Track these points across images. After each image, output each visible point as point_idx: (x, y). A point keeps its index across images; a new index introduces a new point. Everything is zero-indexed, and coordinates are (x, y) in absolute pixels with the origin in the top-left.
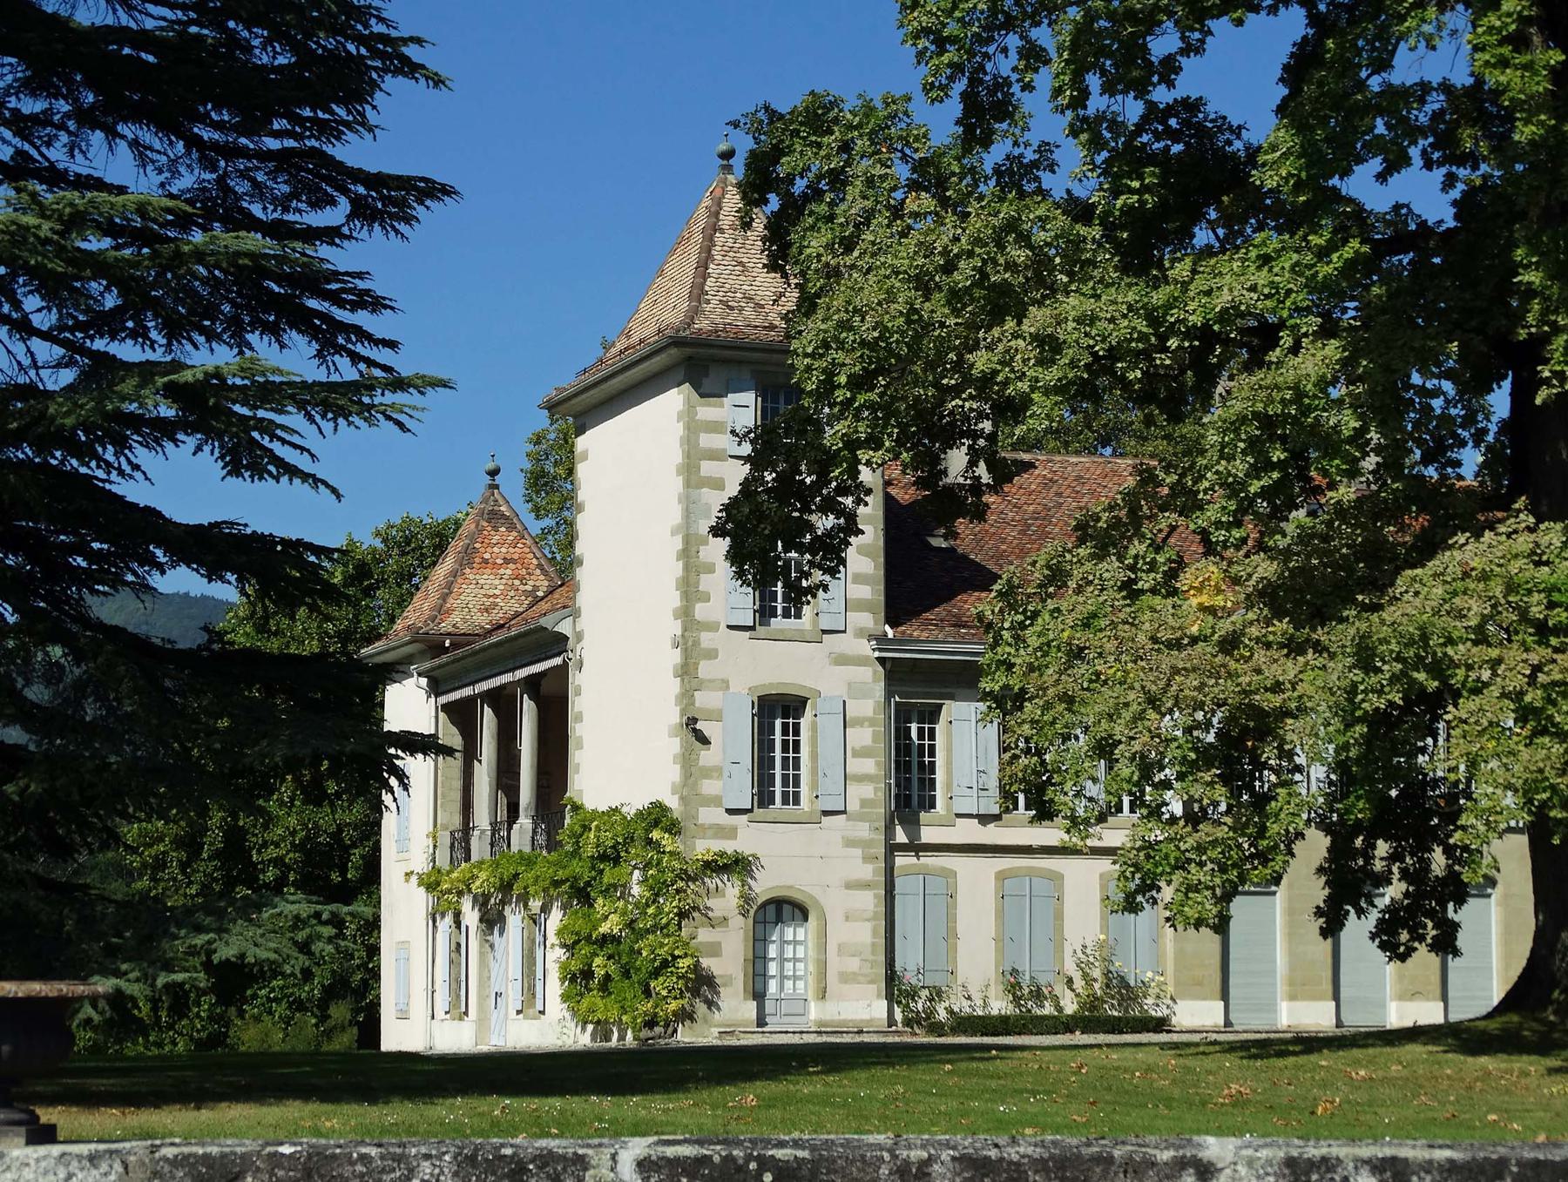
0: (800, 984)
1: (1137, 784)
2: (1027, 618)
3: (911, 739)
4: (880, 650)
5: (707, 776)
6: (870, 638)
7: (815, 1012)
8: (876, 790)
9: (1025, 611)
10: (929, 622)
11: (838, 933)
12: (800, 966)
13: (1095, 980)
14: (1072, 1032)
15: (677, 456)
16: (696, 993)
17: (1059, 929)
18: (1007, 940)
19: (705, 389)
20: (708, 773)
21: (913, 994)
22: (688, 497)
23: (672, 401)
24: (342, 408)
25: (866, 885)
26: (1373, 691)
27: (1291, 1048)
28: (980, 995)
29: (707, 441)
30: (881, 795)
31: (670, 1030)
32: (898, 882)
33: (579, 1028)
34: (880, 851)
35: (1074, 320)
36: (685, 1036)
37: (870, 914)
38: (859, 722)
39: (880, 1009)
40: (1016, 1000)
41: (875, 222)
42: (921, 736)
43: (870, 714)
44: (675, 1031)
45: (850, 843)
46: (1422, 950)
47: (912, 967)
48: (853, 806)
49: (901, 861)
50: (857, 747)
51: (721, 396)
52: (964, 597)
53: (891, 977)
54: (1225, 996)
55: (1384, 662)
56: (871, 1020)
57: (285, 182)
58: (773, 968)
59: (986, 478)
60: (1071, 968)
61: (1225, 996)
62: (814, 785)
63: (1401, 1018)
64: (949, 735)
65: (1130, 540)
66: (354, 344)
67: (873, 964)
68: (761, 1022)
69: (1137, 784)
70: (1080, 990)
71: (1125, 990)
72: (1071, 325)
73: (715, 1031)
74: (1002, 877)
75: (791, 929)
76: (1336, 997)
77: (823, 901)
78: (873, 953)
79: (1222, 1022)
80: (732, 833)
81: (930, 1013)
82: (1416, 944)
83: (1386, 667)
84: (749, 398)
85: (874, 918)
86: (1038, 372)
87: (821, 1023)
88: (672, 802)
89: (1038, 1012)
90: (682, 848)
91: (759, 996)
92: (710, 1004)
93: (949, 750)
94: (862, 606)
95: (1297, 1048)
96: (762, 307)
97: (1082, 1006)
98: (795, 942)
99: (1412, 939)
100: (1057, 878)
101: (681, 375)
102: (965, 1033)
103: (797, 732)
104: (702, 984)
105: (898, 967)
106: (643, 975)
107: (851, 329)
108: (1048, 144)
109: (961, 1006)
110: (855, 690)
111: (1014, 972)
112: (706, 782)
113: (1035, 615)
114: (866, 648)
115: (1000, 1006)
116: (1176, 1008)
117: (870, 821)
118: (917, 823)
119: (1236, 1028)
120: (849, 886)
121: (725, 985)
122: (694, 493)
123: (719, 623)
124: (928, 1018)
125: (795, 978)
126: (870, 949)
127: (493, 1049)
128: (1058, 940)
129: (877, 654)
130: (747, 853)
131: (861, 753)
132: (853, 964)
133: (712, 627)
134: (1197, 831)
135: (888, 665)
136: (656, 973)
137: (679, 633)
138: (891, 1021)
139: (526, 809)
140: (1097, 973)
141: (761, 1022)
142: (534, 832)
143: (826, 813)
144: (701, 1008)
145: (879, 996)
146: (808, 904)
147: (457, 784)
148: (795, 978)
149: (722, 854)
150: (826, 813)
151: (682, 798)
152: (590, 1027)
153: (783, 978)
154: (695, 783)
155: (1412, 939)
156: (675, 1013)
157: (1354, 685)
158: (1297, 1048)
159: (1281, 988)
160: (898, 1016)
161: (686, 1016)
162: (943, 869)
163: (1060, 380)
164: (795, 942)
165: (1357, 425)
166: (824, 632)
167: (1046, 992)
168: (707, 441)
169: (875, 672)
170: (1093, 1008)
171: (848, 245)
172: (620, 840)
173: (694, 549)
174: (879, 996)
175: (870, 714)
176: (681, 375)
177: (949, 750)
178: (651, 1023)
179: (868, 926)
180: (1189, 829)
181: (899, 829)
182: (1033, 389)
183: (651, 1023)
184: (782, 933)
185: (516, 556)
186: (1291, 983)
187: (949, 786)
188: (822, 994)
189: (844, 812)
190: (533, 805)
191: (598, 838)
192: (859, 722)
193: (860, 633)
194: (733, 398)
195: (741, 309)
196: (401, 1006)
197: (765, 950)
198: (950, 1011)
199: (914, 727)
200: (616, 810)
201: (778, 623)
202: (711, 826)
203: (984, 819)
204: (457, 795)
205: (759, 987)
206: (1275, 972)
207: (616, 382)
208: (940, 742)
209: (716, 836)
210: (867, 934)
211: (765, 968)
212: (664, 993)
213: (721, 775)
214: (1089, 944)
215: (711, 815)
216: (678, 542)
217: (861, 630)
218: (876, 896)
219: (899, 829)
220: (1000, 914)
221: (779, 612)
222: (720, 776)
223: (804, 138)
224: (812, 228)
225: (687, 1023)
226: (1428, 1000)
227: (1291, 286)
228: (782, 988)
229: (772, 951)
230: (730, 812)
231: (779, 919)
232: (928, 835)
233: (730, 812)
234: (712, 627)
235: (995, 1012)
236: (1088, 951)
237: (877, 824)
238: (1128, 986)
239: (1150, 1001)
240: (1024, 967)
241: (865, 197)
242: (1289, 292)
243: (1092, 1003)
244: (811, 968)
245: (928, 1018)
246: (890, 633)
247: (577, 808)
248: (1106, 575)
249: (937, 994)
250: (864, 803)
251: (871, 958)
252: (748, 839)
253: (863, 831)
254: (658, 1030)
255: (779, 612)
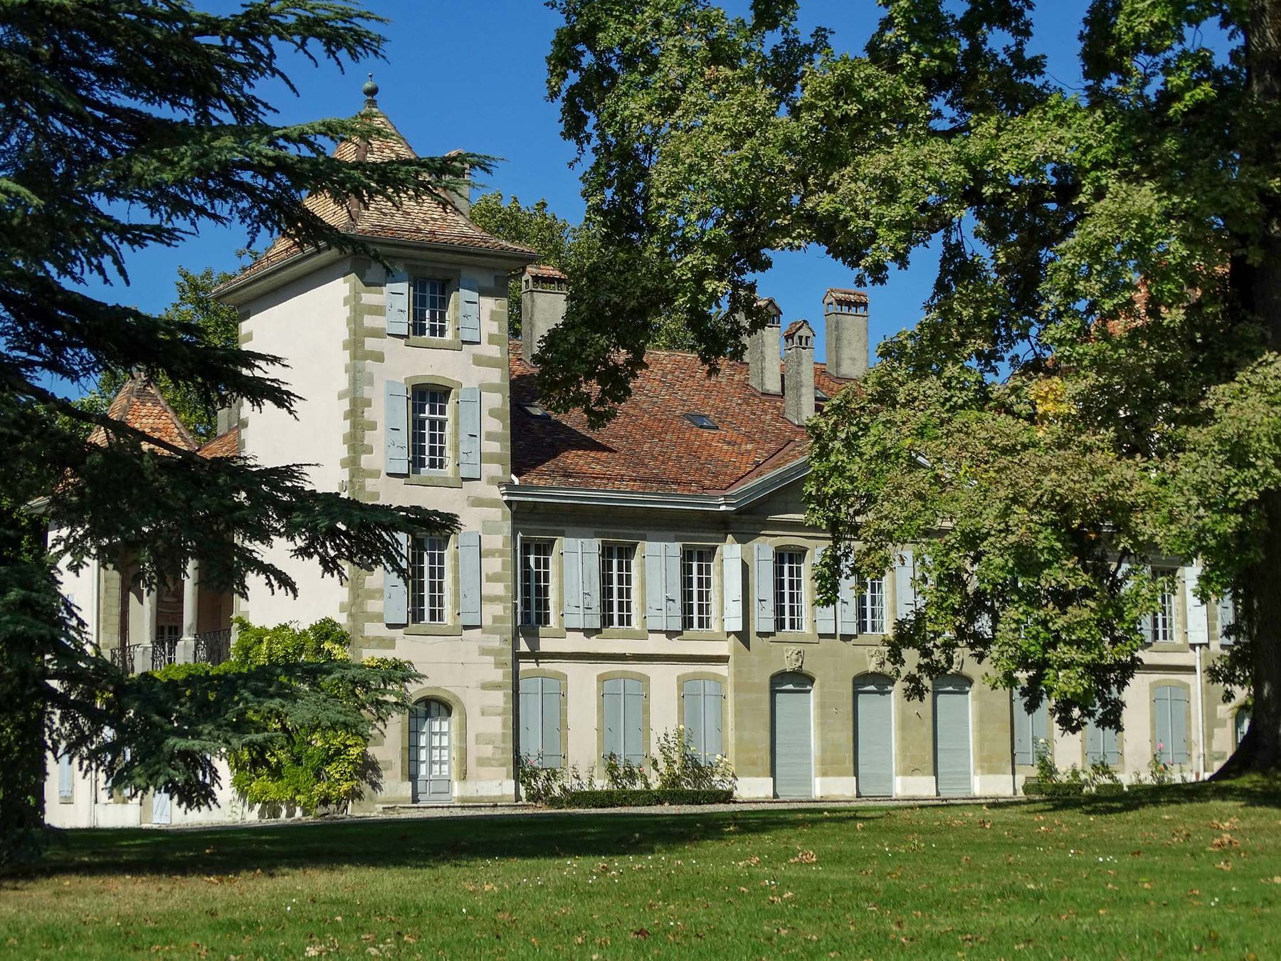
0: (445, 767)
1: (1011, 571)
2: (861, 429)
3: (529, 567)
4: (509, 494)
5: (372, 598)
6: (500, 485)
7: (457, 790)
8: (505, 608)
9: (857, 424)
10: (542, 474)
11: (475, 724)
12: (445, 752)
13: (675, 762)
14: (662, 803)
15: (344, 334)
16: (363, 776)
17: (647, 722)
18: (606, 730)
19: (368, 279)
20: (372, 594)
21: (534, 774)
22: (355, 367)
23: (339, 289)
24: (424, 185)
25: (497, 686)
26: (1246, 484)
27: (1114, 805)
28: (588, 775)
29: (369, 321)
30: (509, 613)
31: (342, 806)
32: (522, 684)
33: (247, 807)
34: (509, 658)
35: (909, 164)
36: (354, 811)
37: (500, 710)
38: (492, 553)
39: (508, 787)
40: (614, 779)
41: (691, 86)
42: (538, 566)
43: (500, 546)
44: (346, 807)
45: (484, 652)
46: (1091, 722)
47: (534, 753)
48: (487, 621)
49: (524, 666)
50: (490, 573)
51: (381, 285)
52: (566, 454)
53: (517, 760)
54: (773, 774)
55: (1257, 458)
56: (503, 796)
57: (111, 56)
58: (423, 755)
59: (746, 323)
60: (655, 752)
61: (773, 774)
62: (456, 605)
63: (904, 789)
64: (561, 563)
65: (944, 362)
66: (189, 195)
67: (504, 750)
68: (415, 799)
69: (1011, 571)
70: (663, 771)
71: (697, 770)
72: (907, 169)
73: (380, 807)
74: (602, 679)
75: (437, 723)
76: (856, 774)
77: (462, 699)
78: (504, 742)
79: (771, 795)
80: (390, 644)
81: (548, 790)
82: (1086, 719)
83: (1259, 463)
84: (403, 287)
85: (504, 713)
86: (883, 209)
87: (462, 799)
88: (341, 619)
89: (630, 787)
90: (350, 656)
91: (413, 777)
92: (375, 785)
93: (561, 576)
94: (491, 458)
95: (1118, 805)
96: (409, 214)
97: (665, 783)
98: (441, 734)
99: (1083, 715)
100: (644, 680)
101: (348, 266)
102: (579, 805)
103: (441, 561)
104: (368, 769)
105: (522, 753)
106: (315, 761)
107: (700, 172)
108: (825, 30)
109: (572, 784)
110: (489, 527)
111: (612, 756)
112: (370, 602)
113: (866, 428)
114: (496, 493)
115: (602, 784)
116: (737, 784)
117: (501, 634)
118: (537, 635)
119: (781, 799)
120: (485, 687)
121: (386, 769)
122: (360, 364)
123: (380, 472)
124: (546, 795)
125: (441, 763)
126: (500, 738)
127: (155, 826)
128: (646, 729)
129: (505, 498)
130: (403, 659)
131: (494, 578)
132: (488, 751)
133: (375, 474)
134: (1065, 613)
135: (514, 508)
136: (329, 760)
137: (347, 478)
138: (518, 798)
139: (189, 629)
140: (676, 757)
141: (415, 799)
142: (196, 646)
143: (466, 627)
144: (366, 788)
145: (508, 777)
146: (452, 701)
147: (116, 610)
148: (441, 763)
149: (384, 661)
150: (466, 627)
151: (350, 615)
152: (258, 806)
153: (432, 763)
154: (362, 603)
155: (1083, 715)
156: (346, 793)
157: (1228, 479)
158: (1118, 805)
159: (814, 767)
160: (523, 793)
161: (355, 795)
162: (556, 673)
163: (903, 216)
164: (441, 734)
165: (1185, 253)
166: (464, 479)
167: (636, 771)
168: (369, 321)
169: (504, 513)
170: (673, 783)
171: (668, 107)
172: (290, 651)
173: (360, 410)
174: (508, 777)
175: (500, 546)
176: (348, 266)
177: (561, 576)
178: (325, 801)
179: (499, 720)
180: (1057, 611)
181: (522, 640)
182: (878, 224)
183: (325, 801)
184: (430, 726)
185: (161, 426)
186: (823, 762)
187: (561, 605)
188: (463, 776)
189: (480, 627)
190: (195, 626)
191: (271, 650)
192: (492, 553)
193: (492, 480)
194: (391, 287)
195: (393, 216)
196: (65, 794)
197: (417, 740)
198: (564, 789)
199: (532, 558)
200: (285, 627)
201: (426, 471)
202: (375, 638)
203: (589, 632)
204: (116, 620)
205: (413, 769)
206: (809, 754)
207: (284, 275)
208: (553, 569)
209: (378, 647)
210: (497, 726)
211: (417, 754)
212: (337, 776)
213: (382, 596)
214: (671, 733)
215: (374, 629)
216: (346, 405)
217: (493, 478)
218: (505, 695)
219: (522, 640)
220: (601, 708)
221: (427, 462)
222: (382, 596)
223: (617, 17)
224: (625, 94)
225: (356, 801)
226: (924, 774)
227: (1091, 142)
228: (430, 772)
229: (423, 741)
230: (390, 626)
231: (428, 715)
232: (546, 645)
233: (390, 626)
234: (375, 474)
235: (598, 788)
236: (670, 739)
237: (505, 637)
238: (700, 768)
239: (717, 778)
240: (620, 752)
241: (680, 65)
242: (1090, 147)
243: (673, 780)
244: (454, 754)
245: (546, 795)
246: (516, 481)
247: (244, 626)
248: (929, 392)
249: (552, 775)
250: (496, 619)
251: (502, 745)
252: (406, 649)
253: (495, 642)
254: (332, 807)
255: (427, 462)
